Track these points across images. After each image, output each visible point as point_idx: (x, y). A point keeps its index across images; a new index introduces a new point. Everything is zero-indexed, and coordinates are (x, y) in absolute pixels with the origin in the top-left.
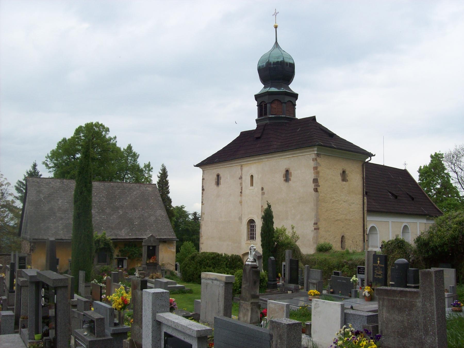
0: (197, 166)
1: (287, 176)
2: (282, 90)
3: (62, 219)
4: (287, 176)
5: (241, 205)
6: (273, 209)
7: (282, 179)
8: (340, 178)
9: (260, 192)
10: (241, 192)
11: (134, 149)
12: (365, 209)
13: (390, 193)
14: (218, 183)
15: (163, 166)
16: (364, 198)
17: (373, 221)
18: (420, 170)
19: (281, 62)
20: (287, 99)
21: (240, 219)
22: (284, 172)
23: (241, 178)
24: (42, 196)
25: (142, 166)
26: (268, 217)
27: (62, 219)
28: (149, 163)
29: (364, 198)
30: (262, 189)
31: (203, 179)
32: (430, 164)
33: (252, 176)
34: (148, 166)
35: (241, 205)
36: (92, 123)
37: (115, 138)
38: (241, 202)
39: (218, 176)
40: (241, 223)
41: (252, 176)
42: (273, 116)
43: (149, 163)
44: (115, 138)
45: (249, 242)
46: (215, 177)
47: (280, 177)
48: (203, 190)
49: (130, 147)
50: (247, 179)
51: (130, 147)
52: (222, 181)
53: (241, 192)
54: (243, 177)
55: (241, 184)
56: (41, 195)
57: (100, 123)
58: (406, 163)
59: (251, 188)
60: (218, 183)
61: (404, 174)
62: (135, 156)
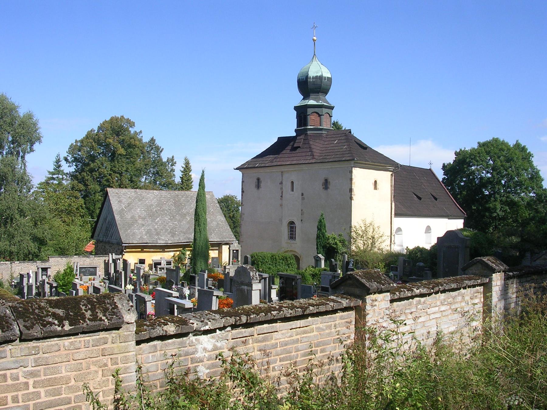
0: (237, 169)
1: (326, 184)
2: (320, 103)
3: (143, 225)
4: (326, 184)
5: (282, 208)
6: (238, 165)
7: (321, 187)
8: (373, 187)
9: (301, 197)
10: (282, 196)
11: (158, 143)
12: (393, 213)
13: (415, 195)
14: (258, 186)
15: (186, 159)
16: (391, 204)
17: (399, 222)
18: (444, 167)
19: (320, 76)
20: (325, 110)
21: (281, 220)
22: (323, 181)
23: (281, 183)
24: (123, 206)
25: (165, 160)
26: (321, 227)
27: (143, 225)
28: (173, 157)
29: (391, 204)
30: (302, 194)
31: (243, 182)
32: (454, 161)
33: (292, 183)
34: (172, 161)
35: (282, 208)
36: (132, 124)
37: (141, 132)
38: (281, 205)
39: (258, 179)
40: (282, 224)
41: (292, 183)
42: (312, 127)
43: (173, 157)
44: (141, 132)
45: (289, 241)
46: (256, 180)
47: (319, 185)
48: (243, 192)
49: (153, 140)
50: (287, 186)
51: (153, 140)
52: (262, 185)
53: (282, 196)
54: (284, 183)
55: (282, 188)
56: (122, 205)
57: (126, 117)
58: (432, 162)
59: (292, 193)
60: (258, 186)
61: (429, 173)
62: (158, 150)
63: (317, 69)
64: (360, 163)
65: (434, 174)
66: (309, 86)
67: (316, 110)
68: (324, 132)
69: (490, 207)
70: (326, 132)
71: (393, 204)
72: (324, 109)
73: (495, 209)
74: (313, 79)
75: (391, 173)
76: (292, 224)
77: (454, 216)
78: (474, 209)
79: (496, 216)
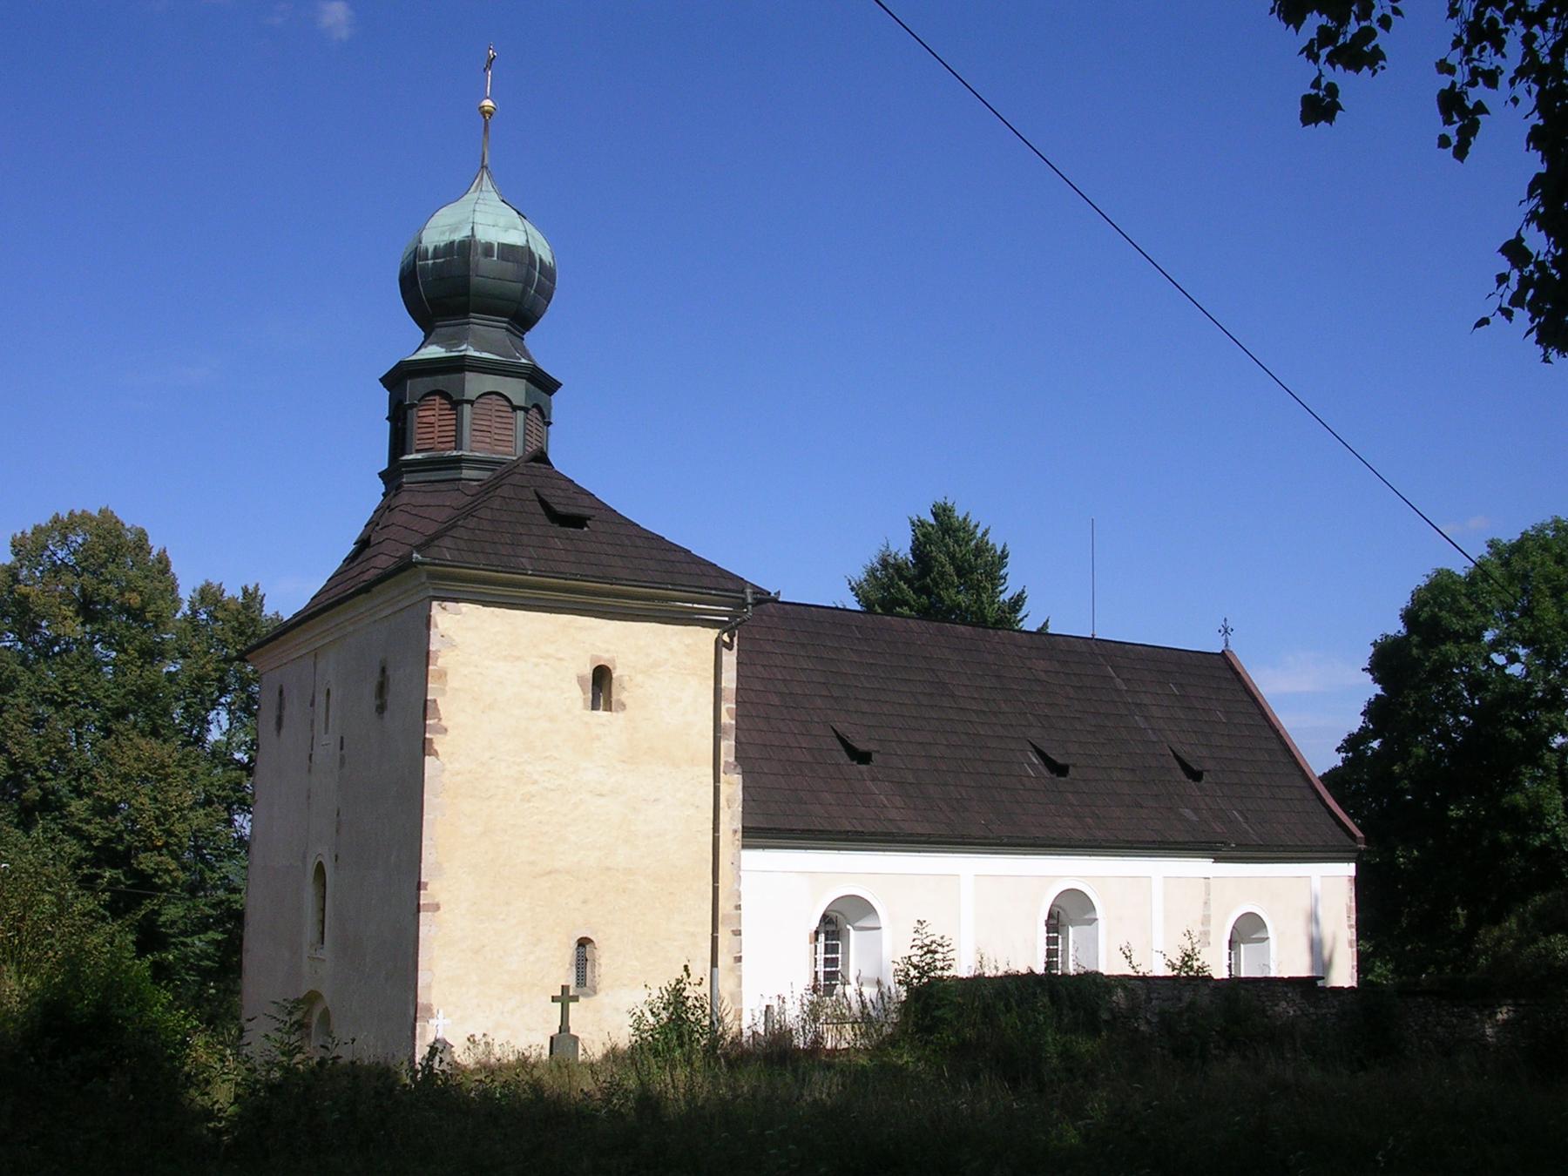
12: (732, 819)
19: (462, 243)
42: (419, 456)
58: (1230, 625)
63: (488, 220)
64: (485, 581)
65: (1237, 674)
66: (444, 290)
67: (441, 381)
68: (466, 473)
69: (1515, 807)
70: (485, 475)
71: (733, 786)
72: (469, 376)
73: (1537, 812)
74: (435, 256)
75: (713, 633)
76: (320, 870)
77: (1259, 847)
78: (1458, 820)
79: (1544, 846)
